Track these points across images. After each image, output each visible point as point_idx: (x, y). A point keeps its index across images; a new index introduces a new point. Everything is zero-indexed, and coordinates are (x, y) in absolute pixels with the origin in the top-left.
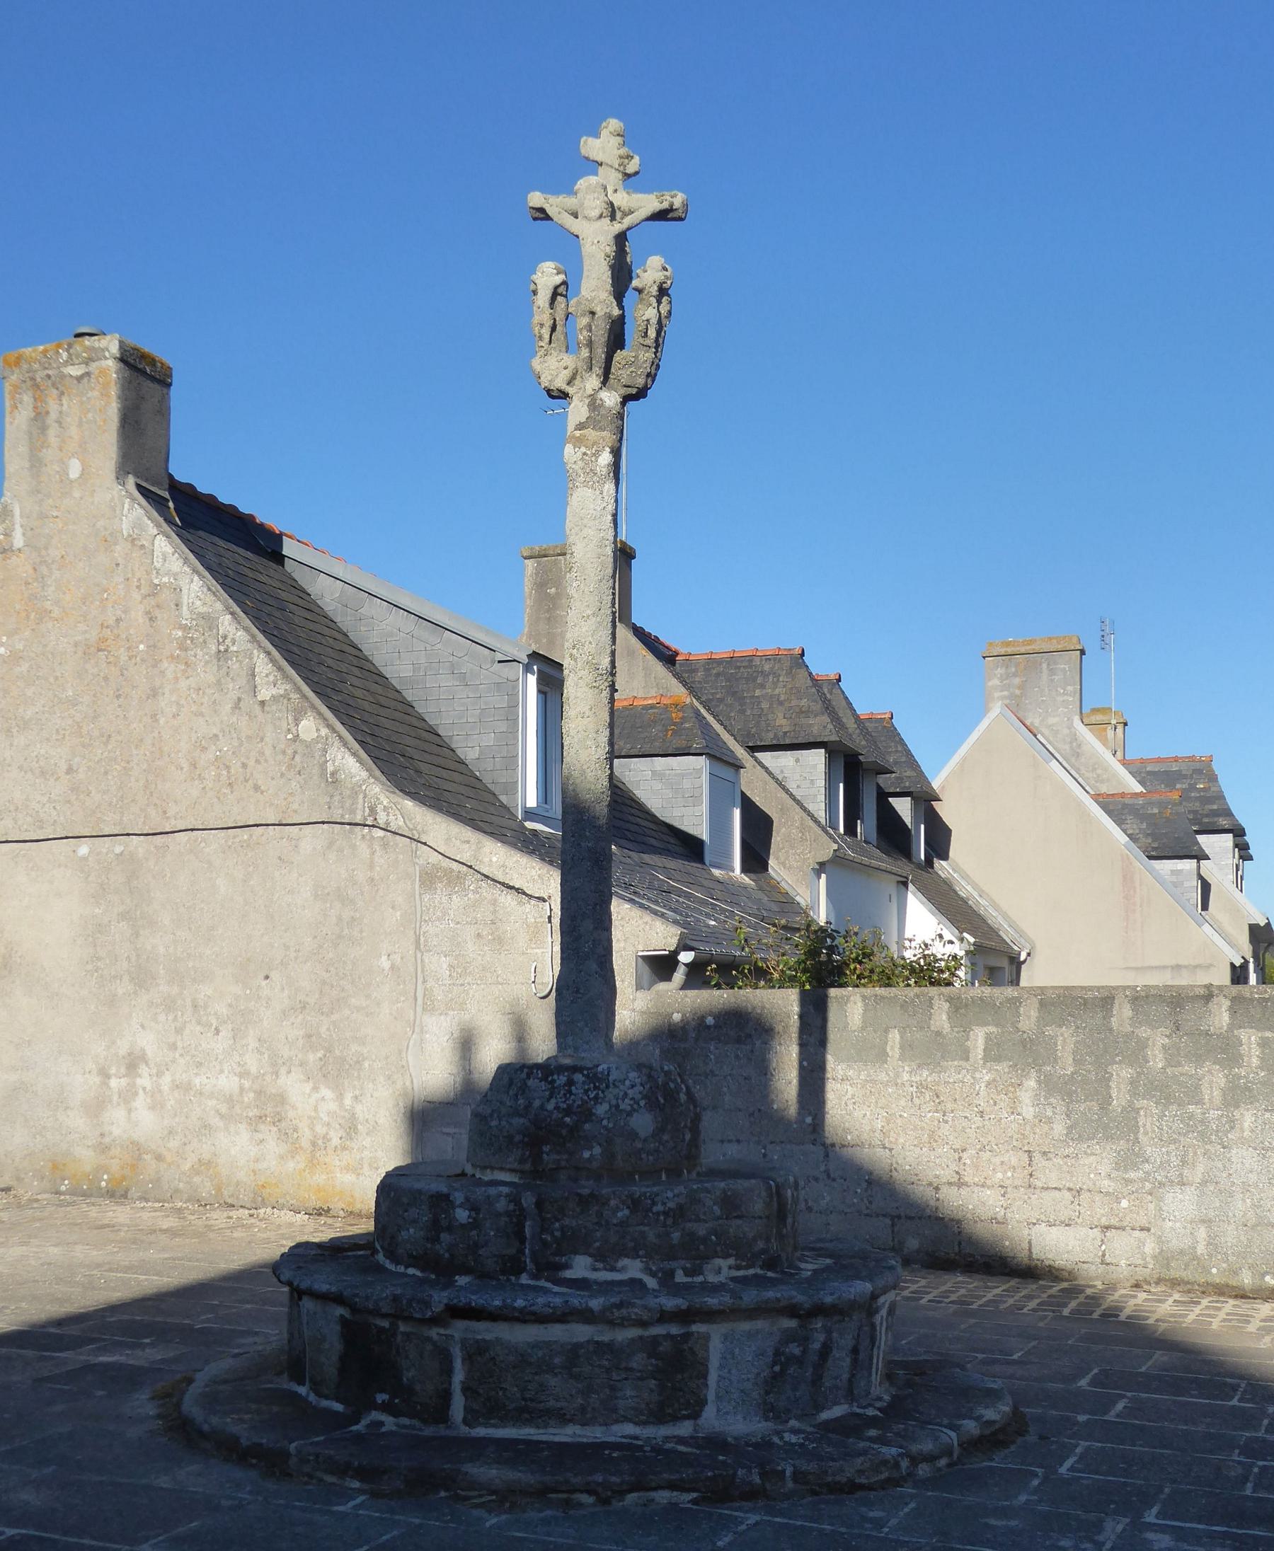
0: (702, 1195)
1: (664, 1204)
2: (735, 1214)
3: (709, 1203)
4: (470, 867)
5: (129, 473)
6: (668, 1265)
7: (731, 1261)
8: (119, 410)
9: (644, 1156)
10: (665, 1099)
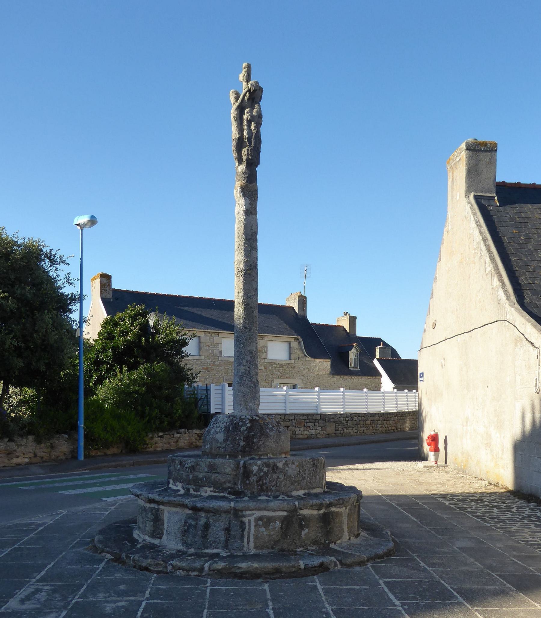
0: (200, 463)
1: (188, 464)
2: (214, 472)
3: (203, 466)
4: (523, 335)
5: (471, 192)
6: (187, 486)
7: (212, 489)
8: (466, 169)
9: (221, 449)
10: (232, 429)
